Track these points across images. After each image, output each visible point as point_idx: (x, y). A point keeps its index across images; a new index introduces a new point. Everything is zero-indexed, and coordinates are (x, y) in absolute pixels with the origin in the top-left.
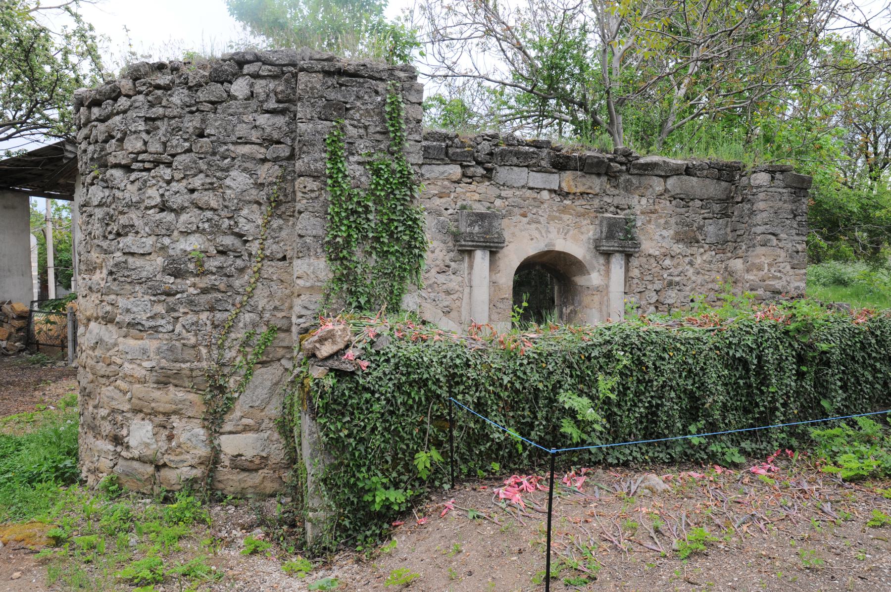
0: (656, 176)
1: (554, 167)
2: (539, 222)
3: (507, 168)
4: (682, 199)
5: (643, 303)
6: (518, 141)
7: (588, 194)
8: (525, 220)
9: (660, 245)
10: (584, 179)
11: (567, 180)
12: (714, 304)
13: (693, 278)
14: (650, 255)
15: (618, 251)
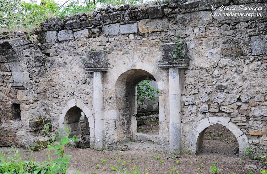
0: (202, 10)
1: (133, 20)
2: (129, 53)
3: (108, 25)
4: (229, 24)
5: (198, 101)
6: (113, 9)
7: (157, 32)
8: (122, 52)
9: (209, 60)
10: (152, 23)
11: (142, 26)
12: (261, 104)
13: (240, 83)
14: (201, 68)
15: (171, 67)
